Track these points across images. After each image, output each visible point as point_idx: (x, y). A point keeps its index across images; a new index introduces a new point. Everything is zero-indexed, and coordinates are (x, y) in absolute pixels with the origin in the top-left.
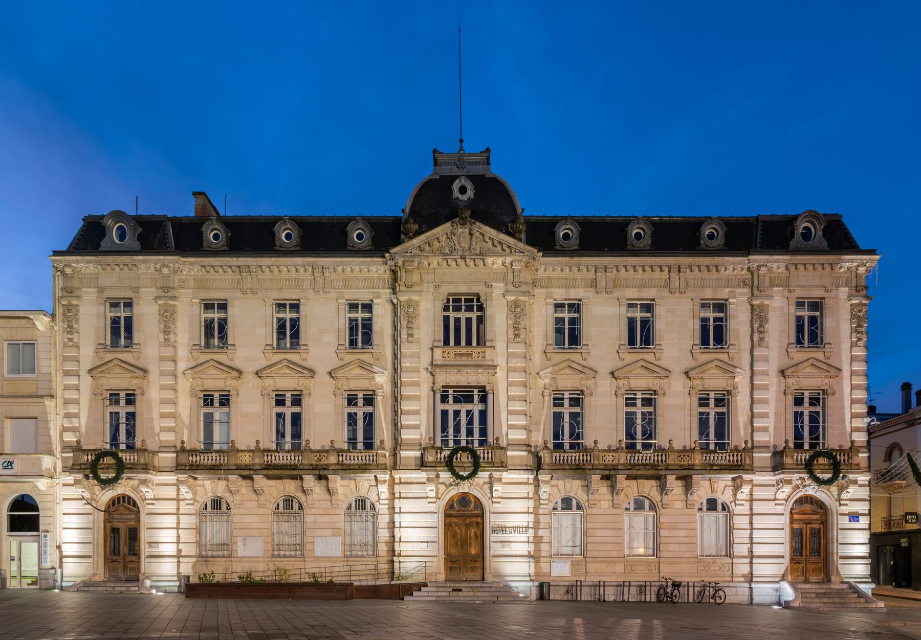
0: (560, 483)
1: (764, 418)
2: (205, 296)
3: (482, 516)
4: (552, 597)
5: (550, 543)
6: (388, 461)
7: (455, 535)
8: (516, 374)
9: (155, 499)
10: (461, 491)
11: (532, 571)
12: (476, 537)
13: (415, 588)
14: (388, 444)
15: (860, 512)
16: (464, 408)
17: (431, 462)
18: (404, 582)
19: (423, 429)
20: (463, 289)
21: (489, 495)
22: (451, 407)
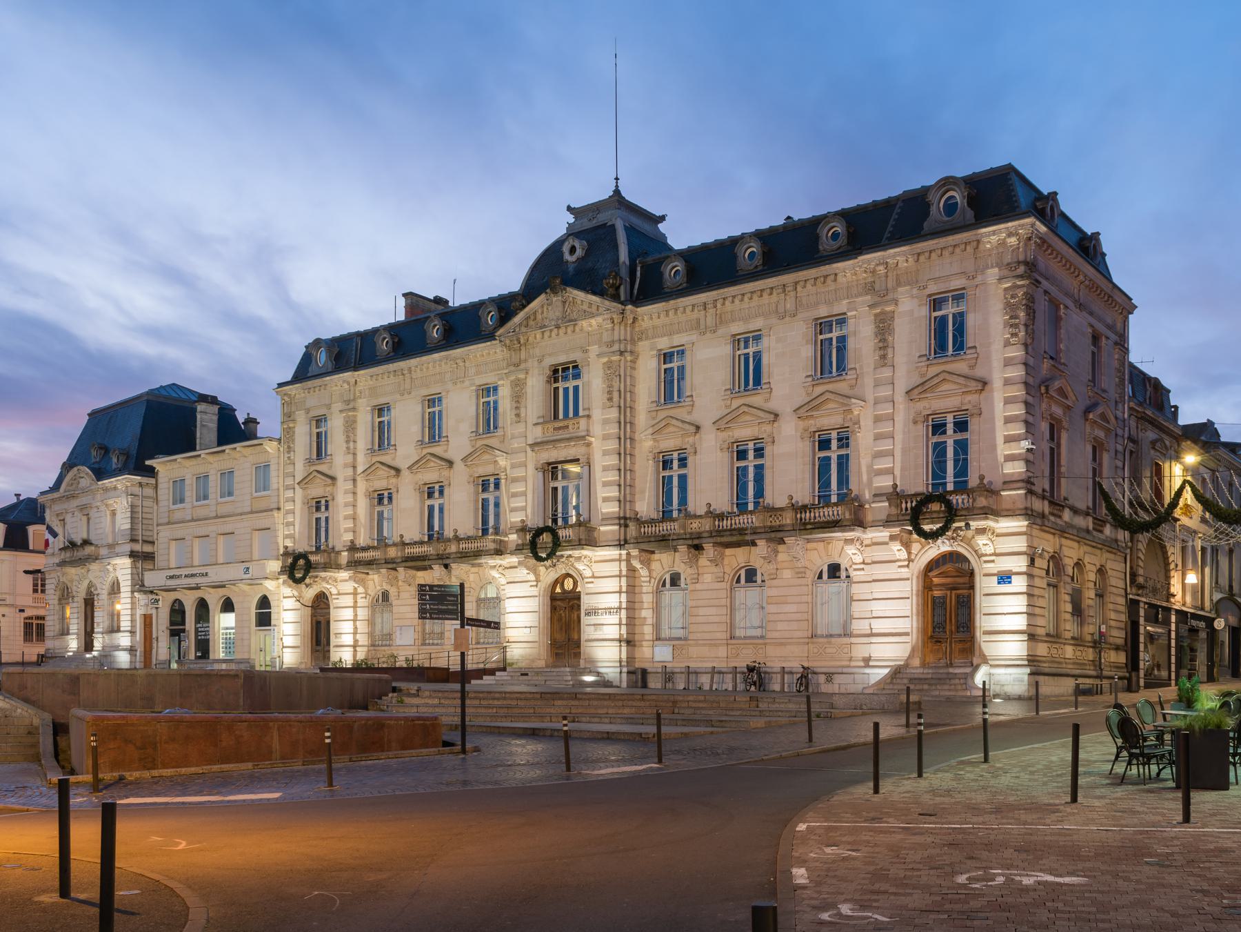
1: (888, 457)
2: (376, 402)
7: (560, 619)
9: (995, 554)
15: (1015, 570)
20: (562, 359)
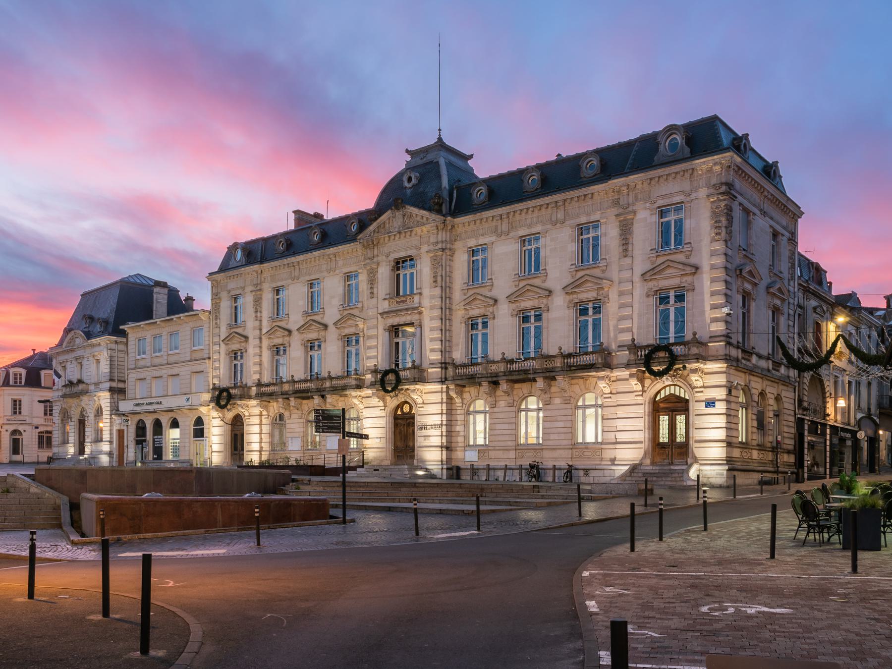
9: (704, 387)
15: (717, 398)
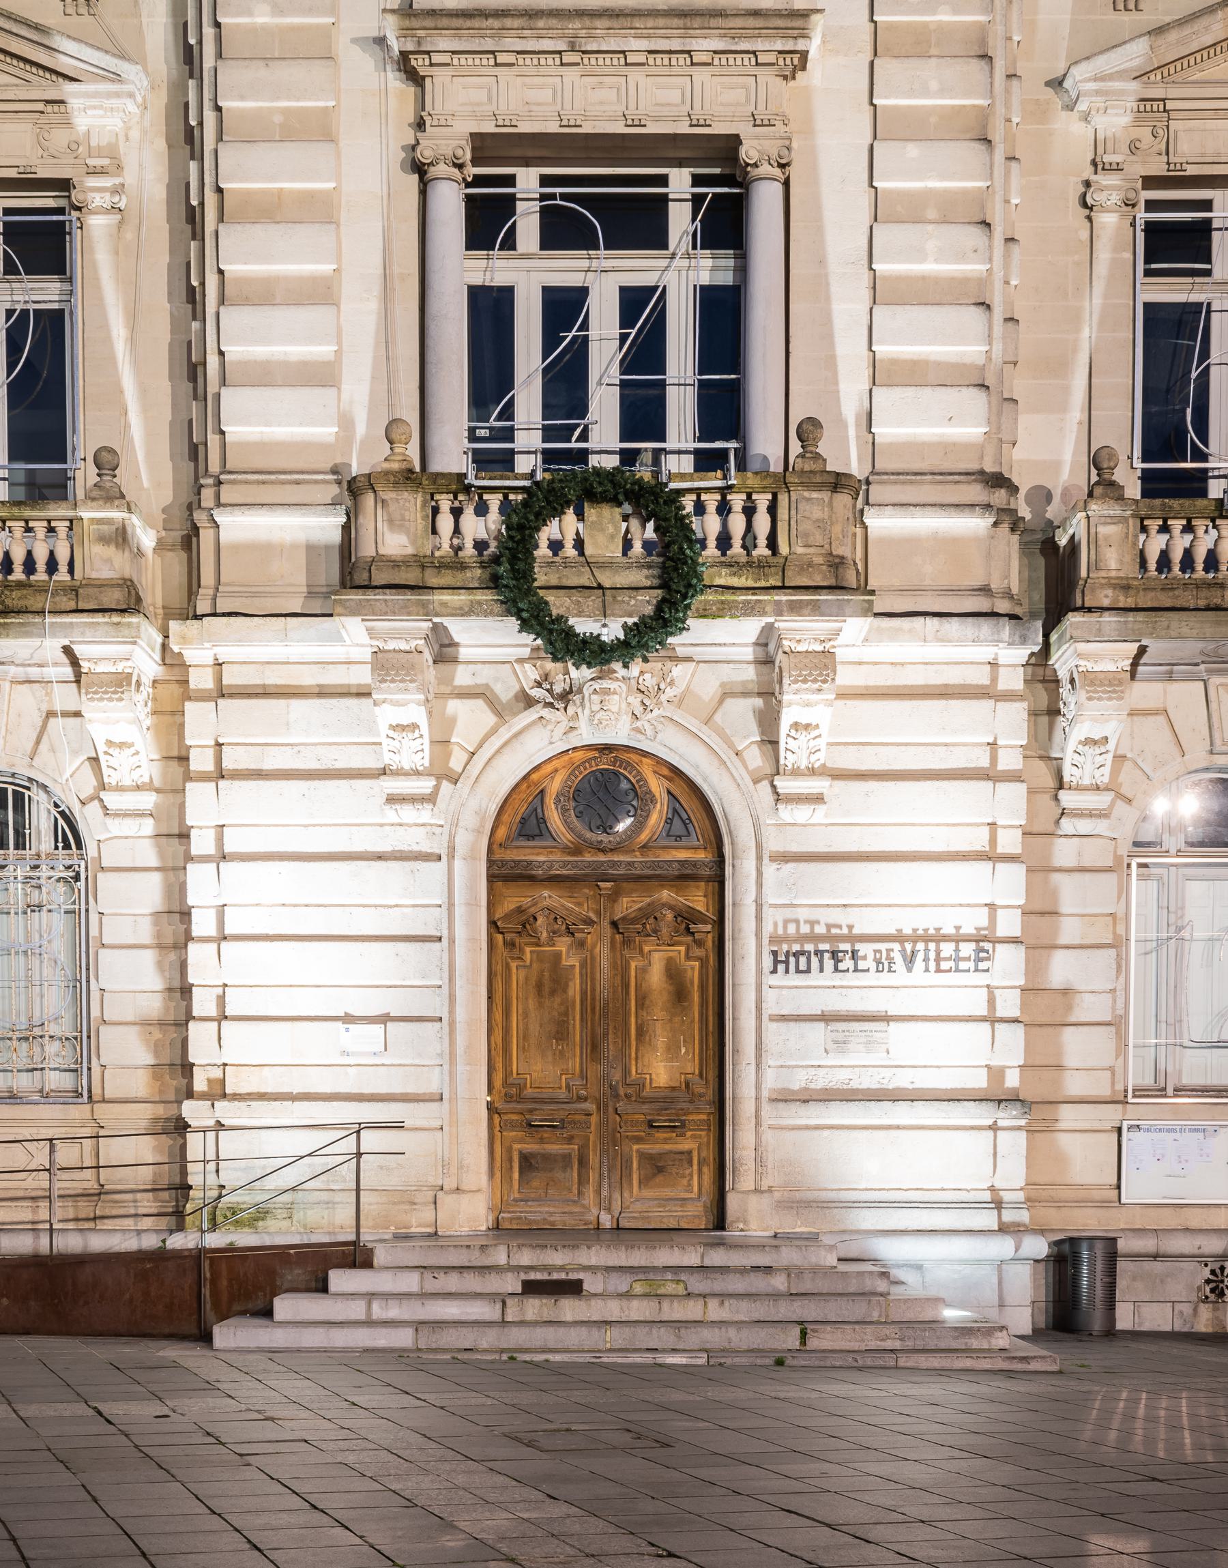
0: (1184, 697)
3: (716, 878)
4: (1125, 1319)
5: (1117, 1024)
6: (157, 577)
7: (551, 982)
8: (930, 71)
10: (587, 735)
11: (1013, 1175)
12: (679, 994)
13: (296, 1274)
14: (150, 471)
16: (604, 276)
17: (394, 564)
18: (245, 1238)
19: (357, 389)
21: (756, 759)
22: (529, 271)
